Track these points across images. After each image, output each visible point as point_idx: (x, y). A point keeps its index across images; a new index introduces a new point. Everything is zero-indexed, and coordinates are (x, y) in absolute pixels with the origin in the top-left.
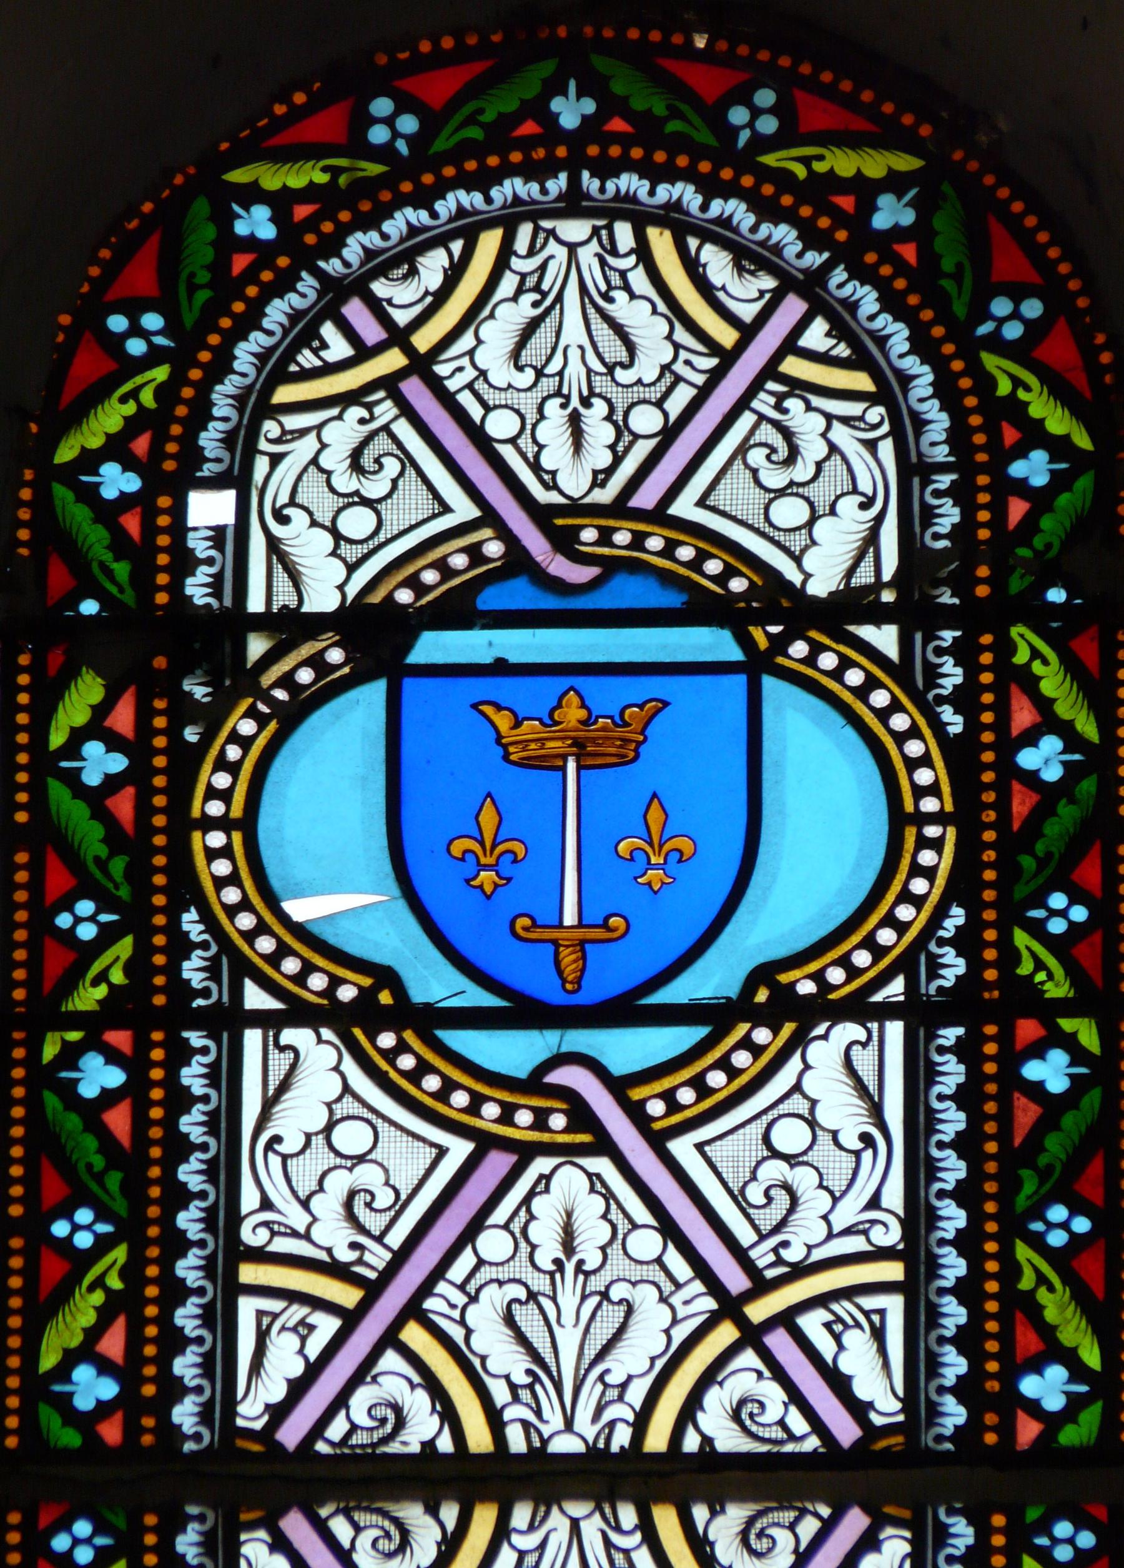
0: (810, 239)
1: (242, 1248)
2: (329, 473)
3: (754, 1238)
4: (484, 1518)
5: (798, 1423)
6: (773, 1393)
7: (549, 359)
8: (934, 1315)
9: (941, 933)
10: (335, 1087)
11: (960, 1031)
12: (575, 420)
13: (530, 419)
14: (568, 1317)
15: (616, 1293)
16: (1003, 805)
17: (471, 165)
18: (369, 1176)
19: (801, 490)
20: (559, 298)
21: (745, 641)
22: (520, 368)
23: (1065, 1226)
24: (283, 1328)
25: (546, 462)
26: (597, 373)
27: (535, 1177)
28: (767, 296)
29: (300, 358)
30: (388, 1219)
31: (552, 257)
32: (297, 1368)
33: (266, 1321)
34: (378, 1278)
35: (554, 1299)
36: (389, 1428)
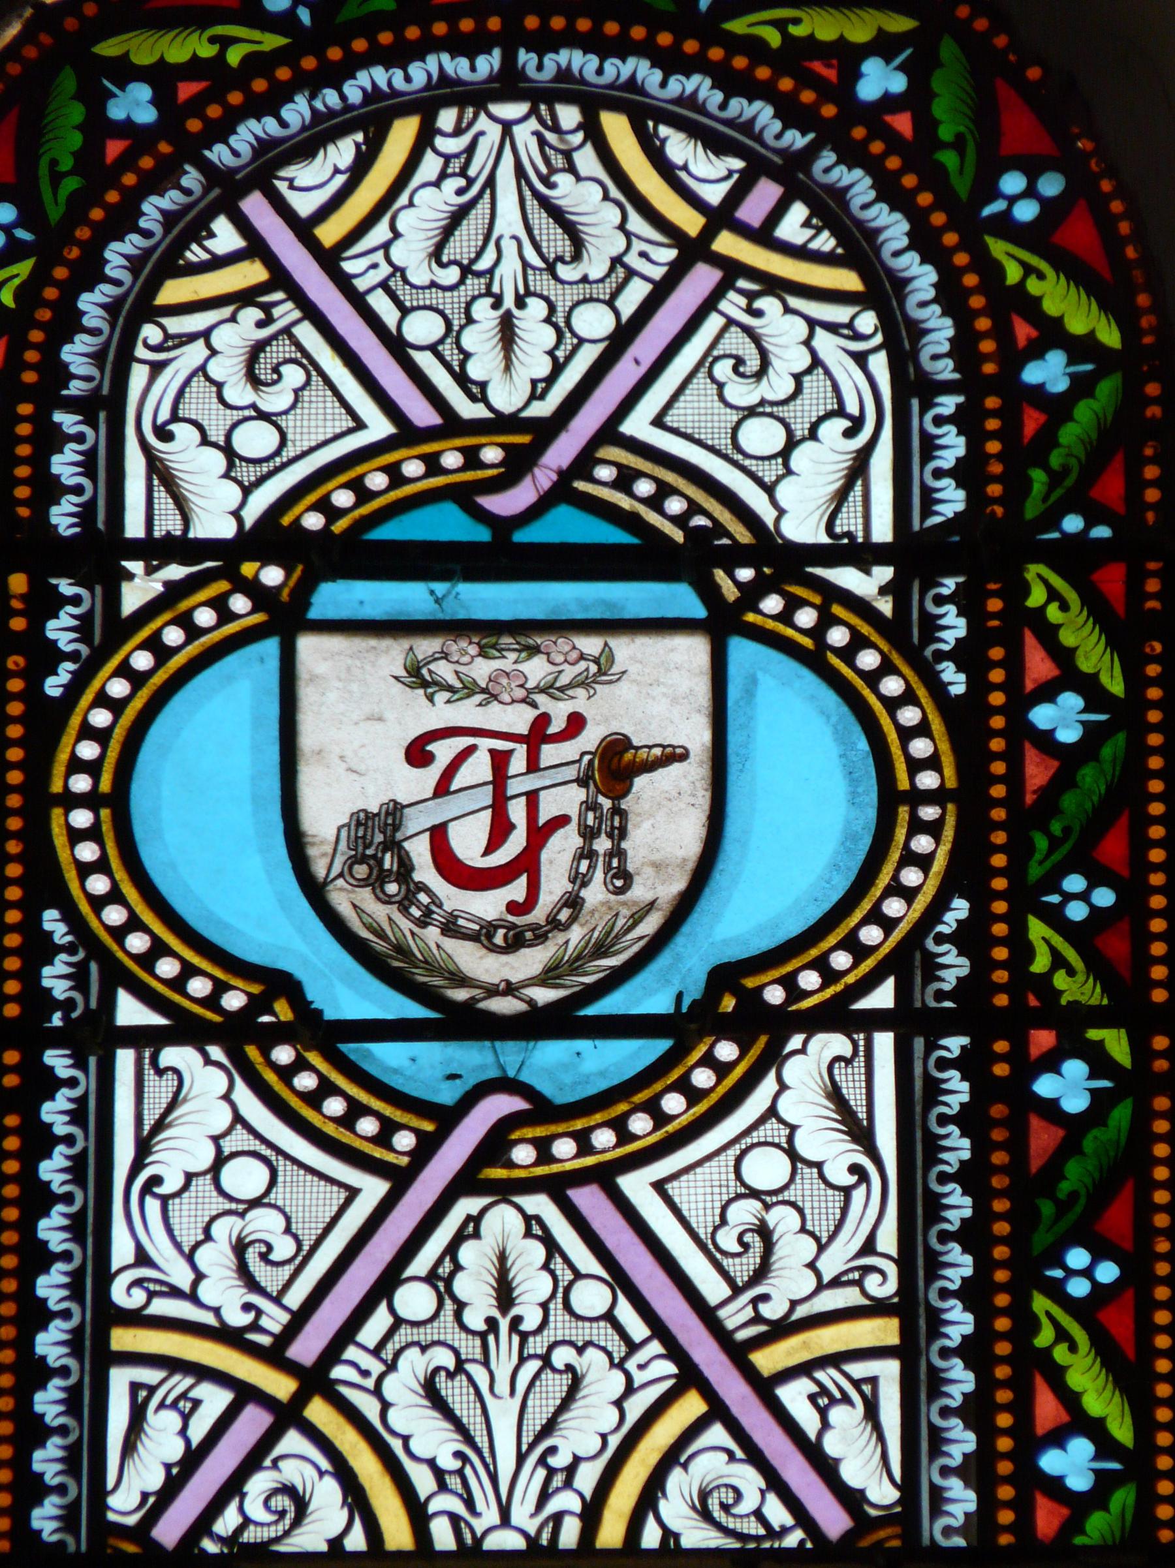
0: (790, 114)
1: (112, 1311)
2: (219, 386)
3: (726, 1292)
4: (611, 1534)
5: (777, 1513)
6: (749, 1479)
7: (479, 254)
8: (937, 1383)
9: (941, 928)
10: (784, 492)
11: (965, 1040)
12: (505, 1294)
13: (557, 1306)
14: (502, 1386)
15: (451, 275)
16: (1014, 779)
17: (385, 38)
18: (742, 393)
19: (234, 1206)
20: (521, 1458)
21: (708, 592)
22: (569, 1368)
23: (1087, 1273)
24: (162, 1405)
25: (538, 1251)
26: (474, 1361)
27: (463, 1217)
28: (736, 176)
29: (188, 254)
30: (720, 346)
31: (482, 133)
32: (175, 1450)
33: (143, 1394)
34: (274, 1344)
35: (525, 265)
36: (290, 1516)
